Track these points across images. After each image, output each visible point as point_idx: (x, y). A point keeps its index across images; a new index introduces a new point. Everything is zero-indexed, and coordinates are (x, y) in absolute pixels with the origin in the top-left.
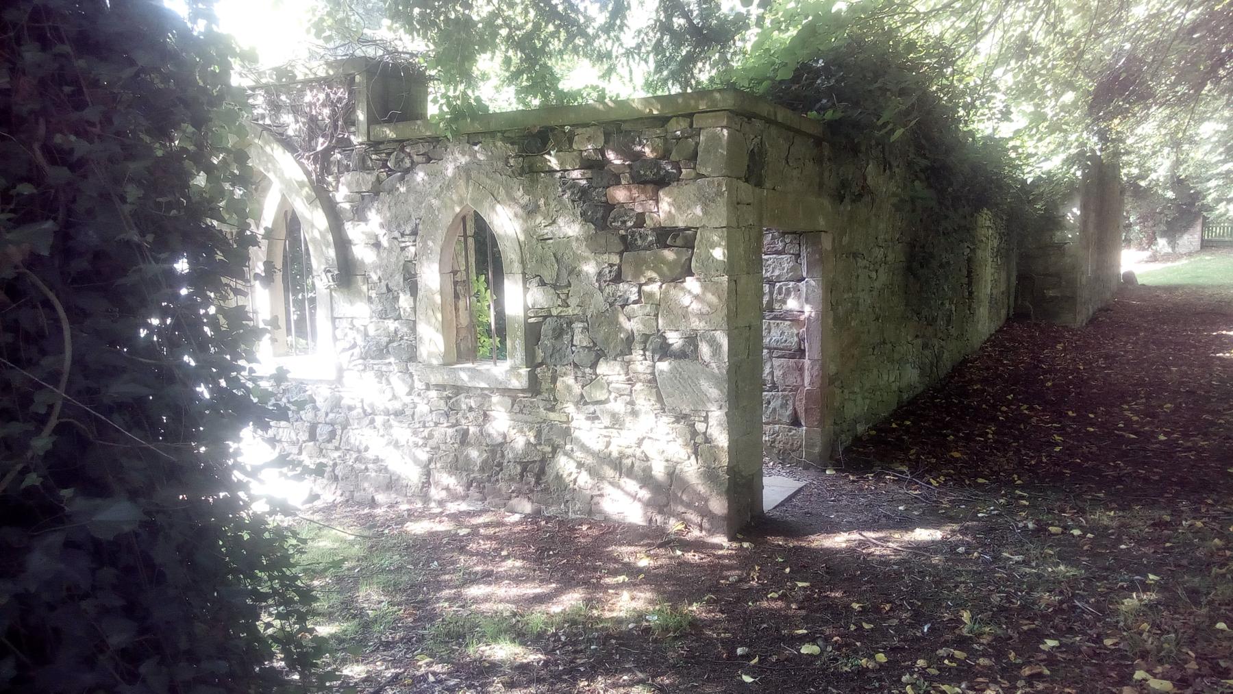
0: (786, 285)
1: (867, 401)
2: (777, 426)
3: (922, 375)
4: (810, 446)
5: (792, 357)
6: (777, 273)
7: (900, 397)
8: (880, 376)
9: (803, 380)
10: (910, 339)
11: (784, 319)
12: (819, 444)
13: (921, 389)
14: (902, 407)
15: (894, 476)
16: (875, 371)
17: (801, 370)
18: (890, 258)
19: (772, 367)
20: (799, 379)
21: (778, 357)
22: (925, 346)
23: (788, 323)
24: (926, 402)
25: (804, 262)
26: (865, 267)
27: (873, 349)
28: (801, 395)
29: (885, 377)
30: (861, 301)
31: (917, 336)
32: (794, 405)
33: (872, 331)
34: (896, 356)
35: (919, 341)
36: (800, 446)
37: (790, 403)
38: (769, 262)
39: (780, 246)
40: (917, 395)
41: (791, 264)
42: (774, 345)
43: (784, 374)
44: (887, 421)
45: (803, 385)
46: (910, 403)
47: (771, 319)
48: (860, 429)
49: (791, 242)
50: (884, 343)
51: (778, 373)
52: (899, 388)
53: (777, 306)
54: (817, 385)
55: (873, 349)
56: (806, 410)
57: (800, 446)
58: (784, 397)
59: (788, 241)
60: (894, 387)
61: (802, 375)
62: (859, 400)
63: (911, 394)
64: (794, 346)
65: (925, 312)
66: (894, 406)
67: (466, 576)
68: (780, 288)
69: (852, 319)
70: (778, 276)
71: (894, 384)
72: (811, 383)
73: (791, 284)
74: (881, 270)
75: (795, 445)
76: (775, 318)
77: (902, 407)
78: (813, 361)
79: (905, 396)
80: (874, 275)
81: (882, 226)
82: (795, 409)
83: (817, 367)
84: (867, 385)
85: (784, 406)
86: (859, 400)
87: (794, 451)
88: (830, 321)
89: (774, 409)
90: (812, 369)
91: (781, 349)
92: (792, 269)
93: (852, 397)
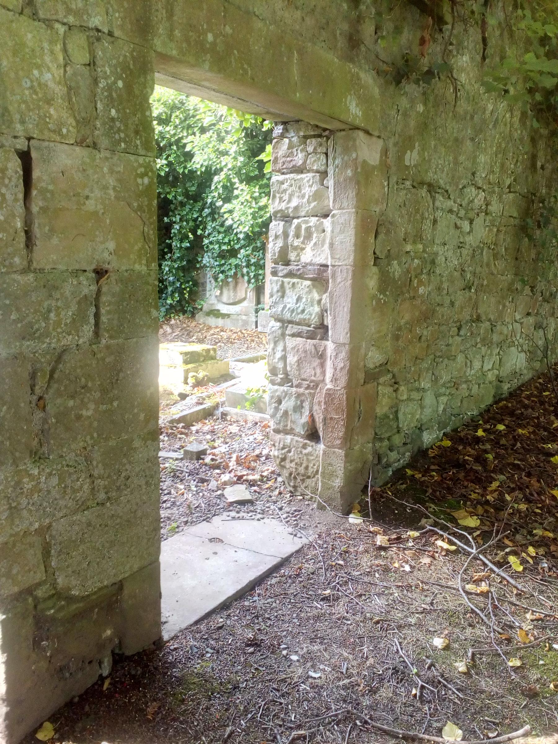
0: (306, 222)
1: (444, 399)
2: (289, 437)
3: (530, 360)
4: (329, 475)
5: (311, 336)
6: (294, 203)
7: (498, 388)
8: (469, 363)
9: (324, 373)
10: (518, 317)
11: (301, 277)
12: (340, 473)
13: (527, 376)
14: (501, 400)
15: (451, 543)
16: (460, 358)
17: (322, 356)
18: (495, 207)
19: (284, 349)
20: (318, 371)
21: (293, 335)
22: (538, 326)
23: (308, 283)
24: (532, 395)
25: (330, 182)
26: (451, 211)
27: (459, 329)
28: (320, 397)
29: (477, 364)
30: (440, 259)
31: (528, 314)
32: (311, 410)
33: (457, 304)
34: (495, 338)
35: (531, 320)
36: (317, 471)
37: (306, 405)
38: (285, 186)
39: (299, 159)
40: (523, 385)
41: (314, 188)
42: (287, 316)
43: (299, 362)
44: (473, 424)
45: (324, 380)
46: (512, 395)
47: (285, 276)
48: (428, 438)
49: (315, 152)
50: (478, 319)
51: (292, 359)
52: (498, 376)
53: (292, 256)
54: (343, 382)
55: (459, 329)
56: (325, 419)
57: (317, 471)
58: (299, 396)
59: (310, 149)
60: (490, 376)
61: (322, 365)
62: (429, 399)
63: (516, 383)
64: (315, 320)
65: (541, 286)
66: (489, 400)
67: (524, 336)
68: (298, 227)
69: (421, 283)
70: (296, 208)
71: (490, 375)
72: (334, 379)
73: (314, 220)
74: (478, 221)
75: (310, 470)
76: (290, 275)
77: (501, 400)
78: (339, 346)
79: (506, 387)
80: (466, 226)
81: (482, 159)
82: (312, 416)
83: (343, 355)
84: (445, 378)
85: (298, 408)
86: (429, 399)
87: (309, 477)
88: (372, 283)
89: (286, 413)
90: (336, 356)
91: (298, 324)
92: (317, 196)
93: (416, 395)
